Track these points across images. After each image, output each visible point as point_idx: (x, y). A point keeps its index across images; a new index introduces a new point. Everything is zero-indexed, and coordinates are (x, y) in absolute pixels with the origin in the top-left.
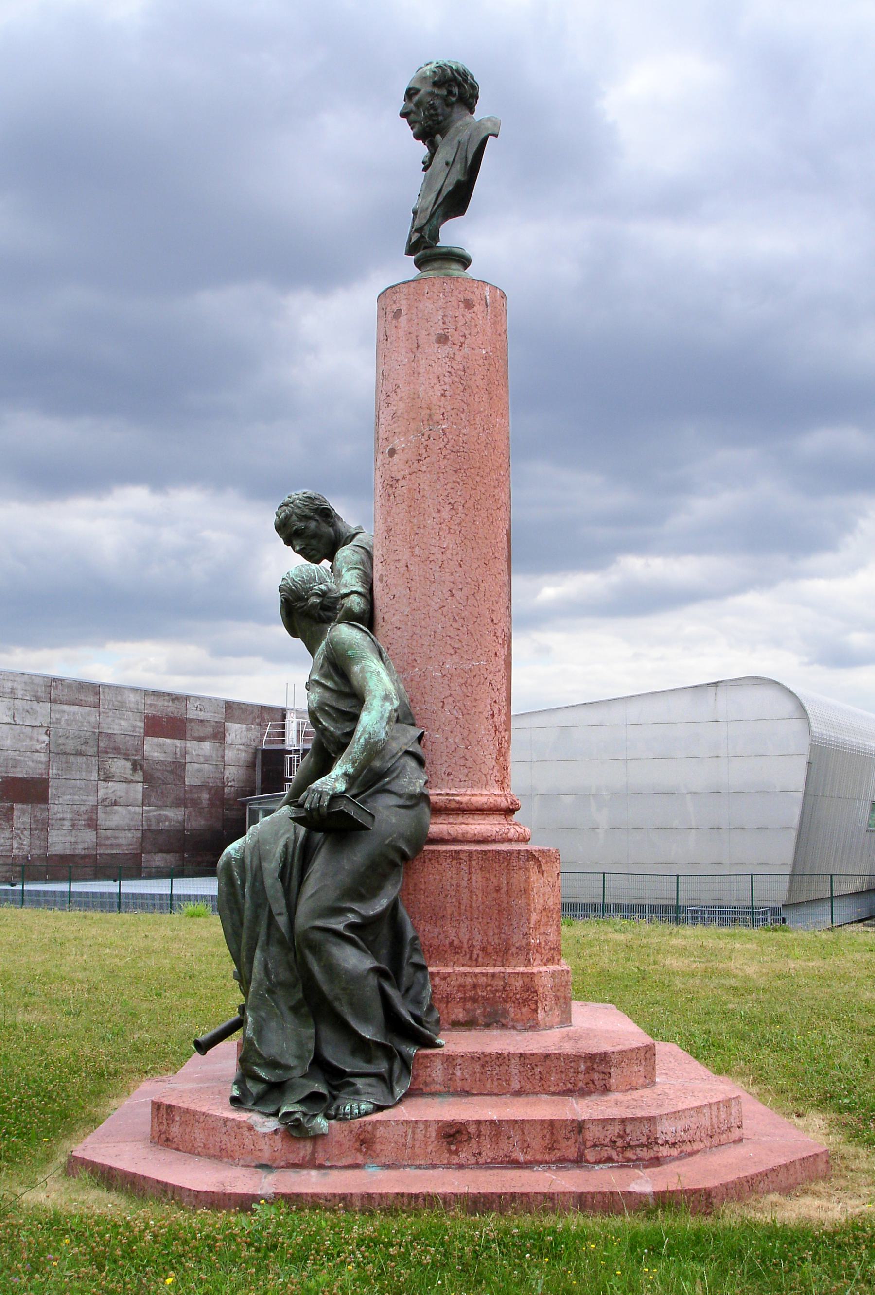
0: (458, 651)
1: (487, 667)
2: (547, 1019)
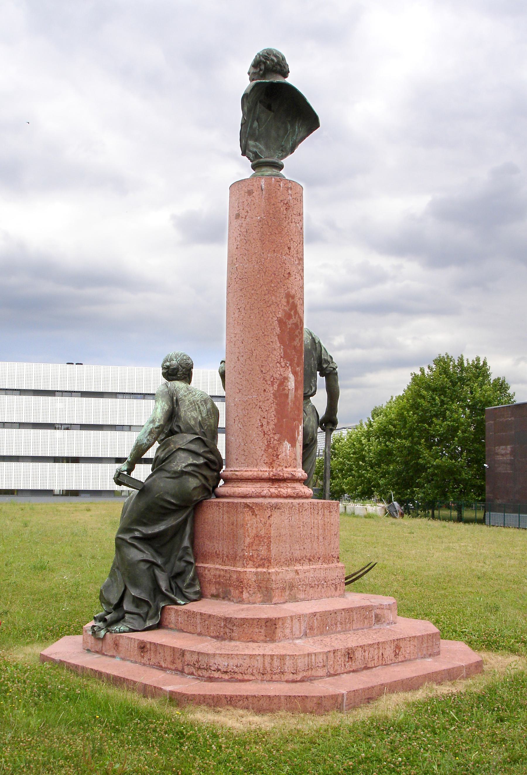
0: (241, 391)
1: (257, 398)
2: (250, 598)
